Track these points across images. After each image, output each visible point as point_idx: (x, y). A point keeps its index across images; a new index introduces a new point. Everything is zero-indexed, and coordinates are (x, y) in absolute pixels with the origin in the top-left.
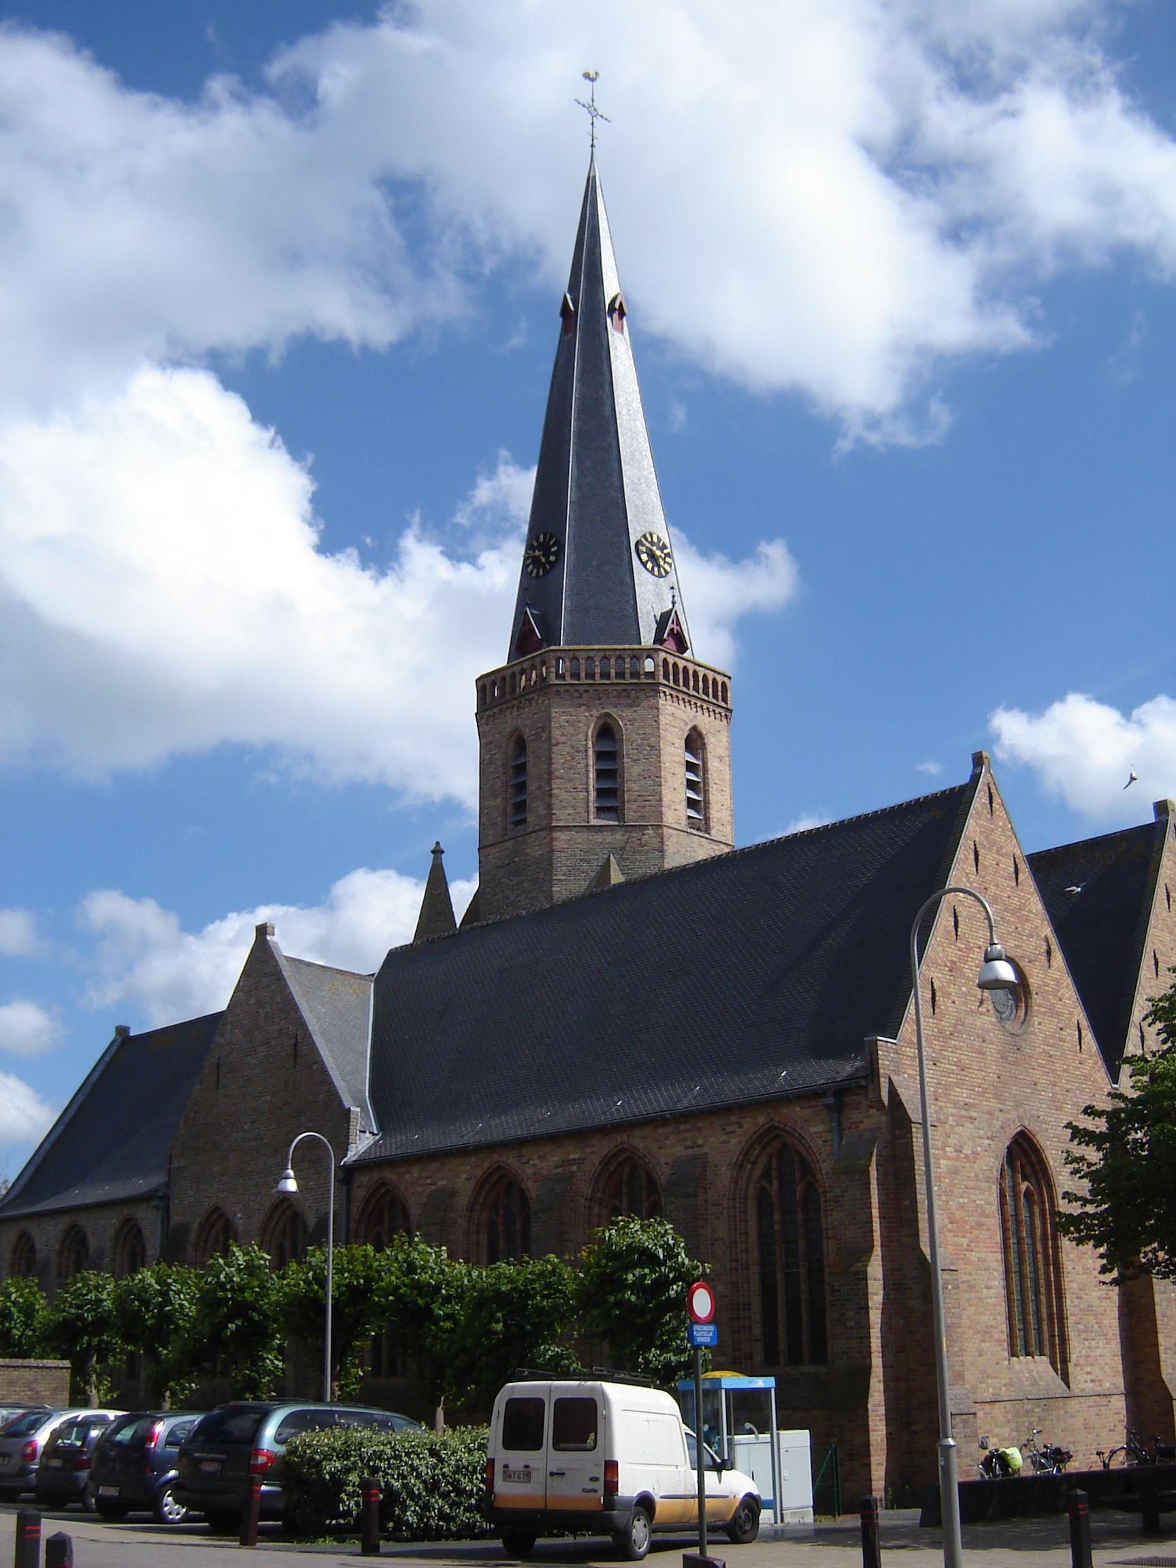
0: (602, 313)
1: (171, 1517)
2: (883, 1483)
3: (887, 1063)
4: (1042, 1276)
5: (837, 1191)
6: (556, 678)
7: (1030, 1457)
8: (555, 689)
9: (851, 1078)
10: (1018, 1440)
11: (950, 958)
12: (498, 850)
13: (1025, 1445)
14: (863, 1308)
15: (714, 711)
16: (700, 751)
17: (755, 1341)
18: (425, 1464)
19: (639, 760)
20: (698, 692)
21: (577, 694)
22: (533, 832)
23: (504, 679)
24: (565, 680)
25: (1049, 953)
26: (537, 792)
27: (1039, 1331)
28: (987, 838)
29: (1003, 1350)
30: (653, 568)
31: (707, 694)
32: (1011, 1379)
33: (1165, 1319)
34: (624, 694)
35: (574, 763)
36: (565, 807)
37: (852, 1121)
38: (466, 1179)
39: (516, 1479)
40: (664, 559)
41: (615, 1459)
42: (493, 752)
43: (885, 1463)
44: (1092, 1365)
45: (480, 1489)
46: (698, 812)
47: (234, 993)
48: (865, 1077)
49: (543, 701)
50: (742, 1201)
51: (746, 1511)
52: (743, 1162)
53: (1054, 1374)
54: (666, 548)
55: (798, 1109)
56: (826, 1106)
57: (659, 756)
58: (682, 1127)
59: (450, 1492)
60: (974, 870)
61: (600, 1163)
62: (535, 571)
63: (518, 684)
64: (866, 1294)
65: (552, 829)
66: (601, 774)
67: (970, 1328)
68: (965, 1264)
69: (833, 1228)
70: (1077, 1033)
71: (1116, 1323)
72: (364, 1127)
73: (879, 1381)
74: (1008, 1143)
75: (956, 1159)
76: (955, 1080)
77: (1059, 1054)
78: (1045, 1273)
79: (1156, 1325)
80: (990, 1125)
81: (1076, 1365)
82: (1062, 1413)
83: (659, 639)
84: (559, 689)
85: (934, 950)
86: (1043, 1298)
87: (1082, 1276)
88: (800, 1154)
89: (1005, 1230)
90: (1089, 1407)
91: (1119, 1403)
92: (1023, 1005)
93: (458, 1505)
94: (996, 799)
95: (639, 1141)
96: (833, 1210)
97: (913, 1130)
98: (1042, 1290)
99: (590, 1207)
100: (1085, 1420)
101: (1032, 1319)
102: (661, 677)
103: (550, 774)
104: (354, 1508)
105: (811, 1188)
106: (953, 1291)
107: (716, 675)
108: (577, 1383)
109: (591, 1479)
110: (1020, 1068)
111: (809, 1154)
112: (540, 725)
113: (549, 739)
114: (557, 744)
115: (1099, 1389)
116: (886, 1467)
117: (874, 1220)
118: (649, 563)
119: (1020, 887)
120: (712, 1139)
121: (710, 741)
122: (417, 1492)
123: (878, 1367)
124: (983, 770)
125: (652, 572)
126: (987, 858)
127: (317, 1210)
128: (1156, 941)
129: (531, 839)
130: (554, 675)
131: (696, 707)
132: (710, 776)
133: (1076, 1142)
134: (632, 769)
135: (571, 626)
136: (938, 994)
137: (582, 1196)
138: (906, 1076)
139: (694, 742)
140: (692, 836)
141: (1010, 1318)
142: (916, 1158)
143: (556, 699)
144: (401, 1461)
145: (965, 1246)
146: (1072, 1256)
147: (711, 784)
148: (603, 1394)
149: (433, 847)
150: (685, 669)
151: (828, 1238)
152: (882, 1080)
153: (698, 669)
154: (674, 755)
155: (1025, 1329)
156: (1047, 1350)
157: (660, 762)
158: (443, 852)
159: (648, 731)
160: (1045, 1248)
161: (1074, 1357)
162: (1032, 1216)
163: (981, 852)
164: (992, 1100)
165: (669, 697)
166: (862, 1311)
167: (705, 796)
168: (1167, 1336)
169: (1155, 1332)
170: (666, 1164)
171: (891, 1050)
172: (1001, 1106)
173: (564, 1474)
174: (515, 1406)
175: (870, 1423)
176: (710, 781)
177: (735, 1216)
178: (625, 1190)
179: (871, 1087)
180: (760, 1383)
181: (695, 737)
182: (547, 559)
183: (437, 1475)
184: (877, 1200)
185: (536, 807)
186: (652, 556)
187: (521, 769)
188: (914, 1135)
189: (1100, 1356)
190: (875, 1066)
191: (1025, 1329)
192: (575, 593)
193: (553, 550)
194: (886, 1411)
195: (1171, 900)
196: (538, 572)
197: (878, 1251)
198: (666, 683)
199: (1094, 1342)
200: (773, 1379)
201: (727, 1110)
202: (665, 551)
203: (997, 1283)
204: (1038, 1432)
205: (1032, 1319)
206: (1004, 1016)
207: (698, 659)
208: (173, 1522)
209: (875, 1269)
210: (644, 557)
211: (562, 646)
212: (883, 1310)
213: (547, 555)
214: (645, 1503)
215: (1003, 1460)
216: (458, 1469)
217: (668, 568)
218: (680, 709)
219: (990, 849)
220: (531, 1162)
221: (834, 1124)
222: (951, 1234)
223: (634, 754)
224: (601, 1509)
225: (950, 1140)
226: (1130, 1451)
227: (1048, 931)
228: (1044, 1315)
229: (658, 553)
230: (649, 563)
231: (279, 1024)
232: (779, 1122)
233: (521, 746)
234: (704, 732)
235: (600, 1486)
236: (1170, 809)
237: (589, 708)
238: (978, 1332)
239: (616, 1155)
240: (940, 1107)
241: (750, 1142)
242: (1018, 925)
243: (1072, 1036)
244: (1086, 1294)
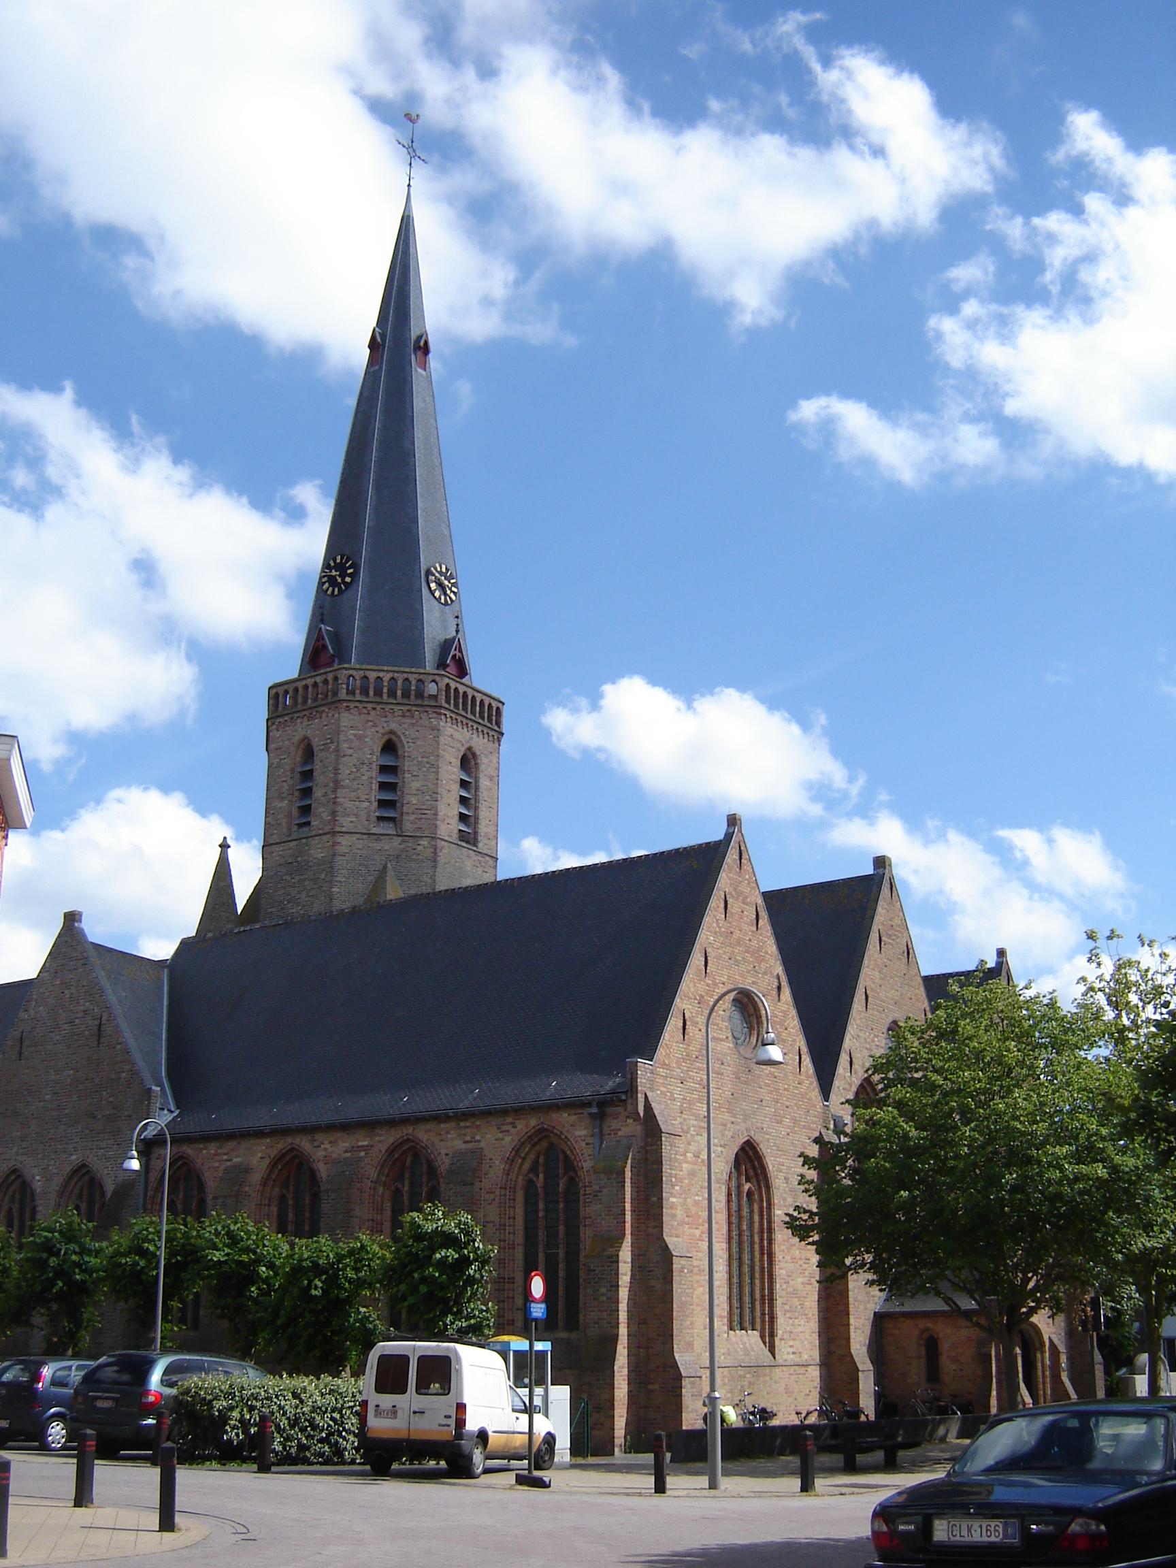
1: (53, 1445)
2: (623, 1431)
3: (644, 1081)
4: (757, 1263)
5: (596, 1187)
6: (347, 694)
7: (741, 1414)
8: (345, 705)
9: (613, 1092)
10: (732, 1400)
11: (699, 992)
12: (281, 849)
13: (737, 1405)
15: (488, 733)
17: (518, 1309)
18: (289, 1404)
20: (475, 716)
21: (365, 711)
22: (316, 836)
23: (296, 690)
24: (355, 697)
25: (779, 988)
26: (323, 798)
27: (753, 1309)
28: (735, 890)
29: (724, 1325)
31: (483, 718)
32: (729, 1349)
33: (856, 1303)
35: (358, 775)
37: (612, 1128)
38: (262, 1158)
39: (385, 1415)
40: (450, 589)
41: (465, 1402)
42: (283, 757)
43: (625, 1415)
44: (794, 1340)
45: (329, 1426)
46: (468, 826)
47: (40, 972)
48: (626, 1092)
49: (333, 715)
50: (512, 1190)
51: (546, 1446)
52: (515, 1157)
53: (762, 1345)
55: (565, 1115)
56: (591, 1114)
57: (437, 773)
58: (462, 1124)
59: (307, 1427)
60: (723, 916)
61: (386, 1151)
62: (331, 589)
64: (617, 1274)
65: (334, 833)
67: (698, 1305)
68: (697, 1251)
69: (591, 1218)
70: (798, 1057)
71: (815, 1305)
72: (162, 1105)
73: (624, 1348)
74: (736, 1150)
75: (694, 1163)
76: (697, 1097)
77: (782, 1075)
78: (760, 1261)
79: (848, 1308)
80: (723, 1135)
81: (781, 1339)
82: (768, 1378)
83: (442, 665)
84: (348, 704)
85: (687, 986)
86: (757, 1282)
87: (790, 1265)
88: (564, 1153)
89: (730, 1223)
90: (791, 1374)
91: (815, 1373)
92: (756, 1032)
93: (312, 1437)
94: (744, 856)
95: (423, 1134)
96: (591, 1202)
97: (663, 1139)
98: (757, 1275)
99: (375, 1189)
100: (786, 1385)
101: (747, 1299)
102: (443, 702)
104: (235, 1438)
105: (572, 1182)
106: (688, 1275)
107: (492, 701)
108: (435, 1344)
109: (445, 1417)
110: (750, 1087)
111: (573, 1154)
112: (329, 736)
113: (337, 750)
114: (345, 756)
117: (627, 1213)
119: (759, 931)
120: (488, 1136)
122: (282, 1427)
123: (623, 1336)
124: (736, 830)
125: (439, 600)
126: (734, 906)
127: (116, 1177)
128: (867, 980)
130: (345, 691)
132: (480, 794)
133: (806, 1167)
134: (412, 785)
136: (688, 1023)
137: (368, 1179)
138: (659, 1092)
140: (461, 848)
141: (730, 1298)
142: (664, 1163)
143: (346, 714)
144: (272, 1402)
145: (698, 1236)
146: (783, 1247)
148: (456, 1352)
150: (465, 694)
151: (585, 1226)
152: (639, 1095)
153: (476, 694)
154: (451, 773)
155: (741, 1307)
156: (758, 1326)
158: (229, 847)
160: (762, 1240)
161: (780, 1332)
162: (751, 1212)
163: (730, 901)
164: (727, 1114)
165: (449, 720)
166: (613, 1289)
167: (475, 812)
168: (857, 1318)
169: (848, 1314)
170: (447, 1155)
171: (648, 1071)
172: (733, 1119)
173: (424, 1412)
174: (383, 1359)
175: (616, 1382)
177: (505, 1203)
178: (407, 1175)
179: (629, 1101)
181: (470, 756)
182: (343, 580)
183: (299, 1413)
184: (630, 1196)
187: (308, 775)
188: (663, 1143)
189: (801, 1332)
190: (635, 1083)
191: (741, 1307)
193: (349, 571)
194: (628, 1371)
195: (883, 943)
196: (333, 591)
197: (628, 1239)
198: (447, 706)
199: (797, 1320)
200: (550, 1343)
201: (504, 1112)
202: (452, 581)
203: (721, 1268)
204: (748, 1394)
205: (747, 1299)
206: (739, 1042)
207: (476, 684)
208: (55, 1449)
209: (625, 1254)
210: (433, 586)
213: (343, 576)
214: (483, 1436)
216: (314, 1409)
217: (453, 597)
218: (458, 731)
219: (737, 899)
220: (322, 1146)
221: (597, 1130)
222: (687, 1226)
224: (452, 1439)
225: (691, 1147)
226: (821, 1413)
227: (779, 969)
228: (758, 1296)
229: (446, 583)
231: (84, 1005)
233: (309, 753)
234: (478, 753)
235: (452, 1422)
239: (401, 1144)
240: (685, 1120)
241: (522, 1140)
242: (756, 964)
243: (794, 1060)
244: (793, 1280)
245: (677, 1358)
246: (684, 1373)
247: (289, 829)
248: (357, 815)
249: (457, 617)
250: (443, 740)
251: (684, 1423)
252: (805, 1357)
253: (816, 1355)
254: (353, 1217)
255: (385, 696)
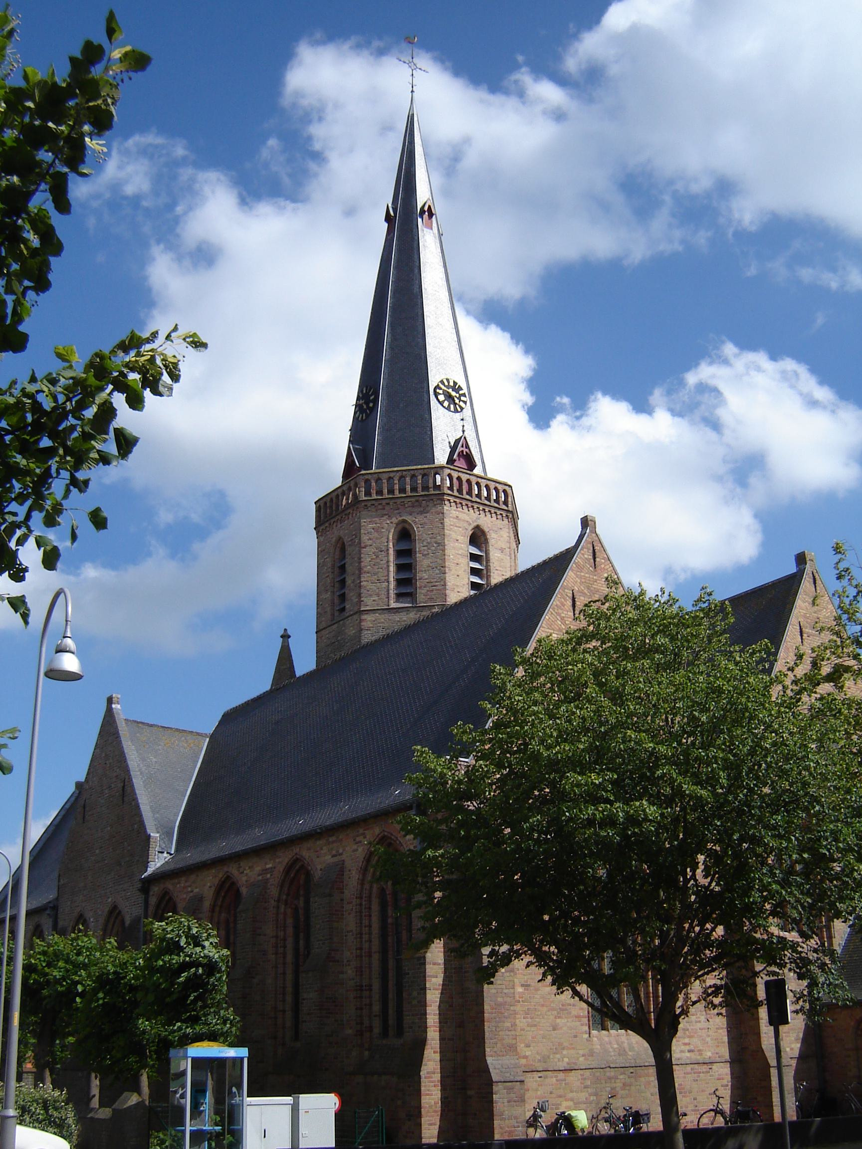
0: (415, 216)
14: (421, 989)
16: (483, 545)
19: (428, 554)
21: (380, 507)
22: (348, 617)
24: (371, 496)
28: (588, 588)
30: (449, 405)
34: (417, 504)
35: (378, 560)
36: (371, 595)
40: (459, 399)
43: (438, 1123)
44: (690, 1037)
54: (462, 389)
57: (444, 550)
58: (331, 839)
63: (340, 503)
66: (400, 568)
83: (451, 461)
95: (306, 852)
103: (360, 569)
107: (497, 485)
114: (365, 547)
115: (700, 1059)
116: (440, 1127)
118: (446, 402)
121: (492, 537)
123: (433, 1039)
125: (448, 409)
129: (348, 622)
131: (479, 511)
132: (491, 564)
134: (423, 562)
135: (380, 454)
139: (478, 538)
143: (364, 513)
147: (492, 571)
149: (282, 632)
157: (445, 555)
158: (289, 637)
159: (435, 531)
175: (422, 1088)
176: (492, 568)
178: (302, 892)
180: (231, 1052)
181: (480, 534)
185: (351, 595)
186: (449, 397)
187: (343, 568)
192: (385, 429)
195: (805, 636)
202: (461, 392)
207: (490, 475)
210: (441, 398)
211: (374, 470)
212: (442, 990)
215: (568, 1121)
223: (424, 550)
229: (453, 394)
230: (446, 402)
232: (388, 832)
234: (486, 530)
236: (807, 559)
237: (390, 517)
238: (553, 1009)
245: (488, 1062)
246: (495, 1077)
247: (333, 615)
248: (378, 595)
249: (462, 420)
250: (447, 521)
251: (496, 1131)
252: (709, 1054)
253: (725, 1052)
254: (260, 935)
255: (397, 492)
